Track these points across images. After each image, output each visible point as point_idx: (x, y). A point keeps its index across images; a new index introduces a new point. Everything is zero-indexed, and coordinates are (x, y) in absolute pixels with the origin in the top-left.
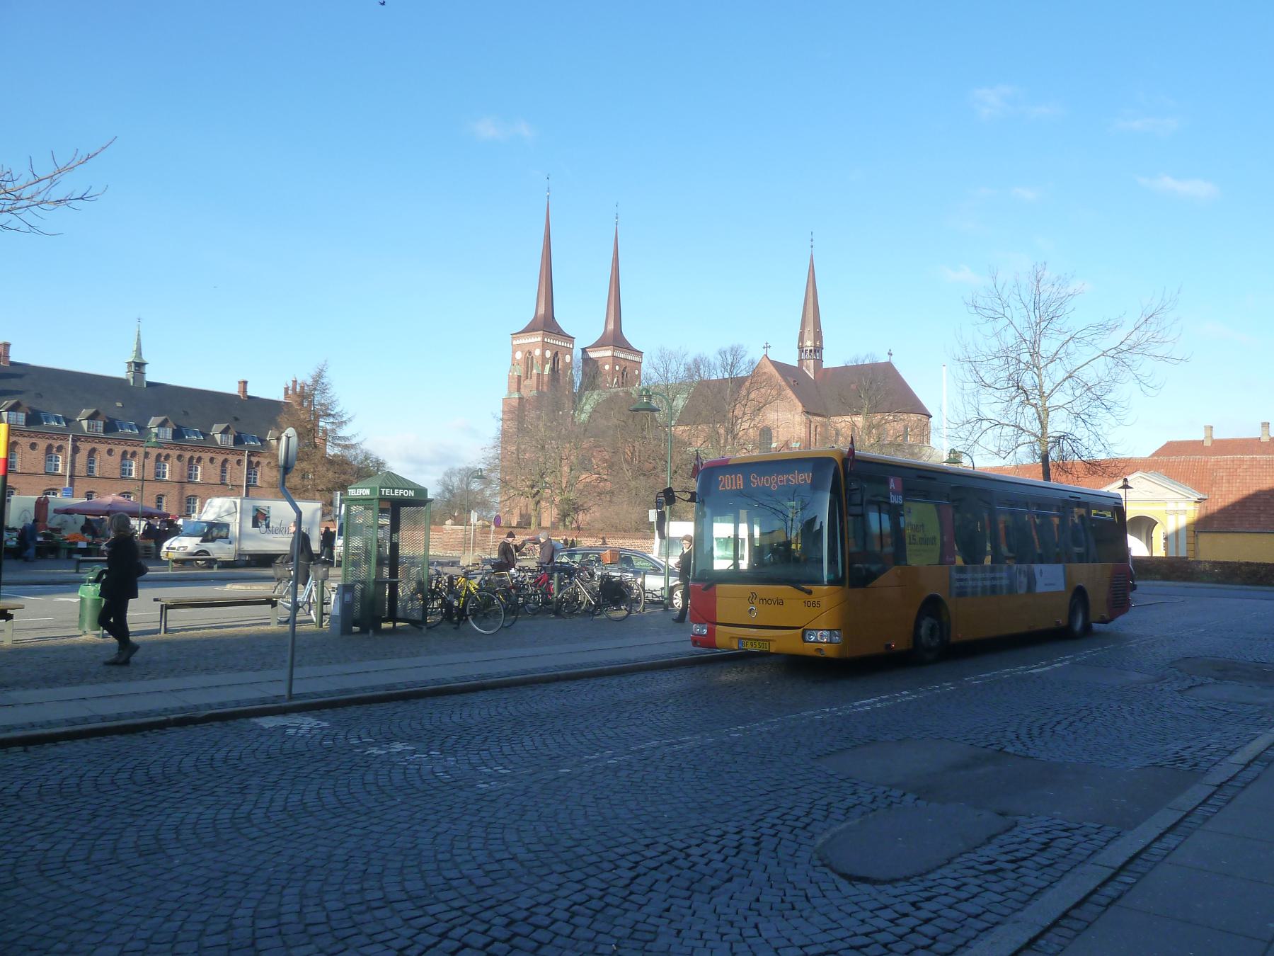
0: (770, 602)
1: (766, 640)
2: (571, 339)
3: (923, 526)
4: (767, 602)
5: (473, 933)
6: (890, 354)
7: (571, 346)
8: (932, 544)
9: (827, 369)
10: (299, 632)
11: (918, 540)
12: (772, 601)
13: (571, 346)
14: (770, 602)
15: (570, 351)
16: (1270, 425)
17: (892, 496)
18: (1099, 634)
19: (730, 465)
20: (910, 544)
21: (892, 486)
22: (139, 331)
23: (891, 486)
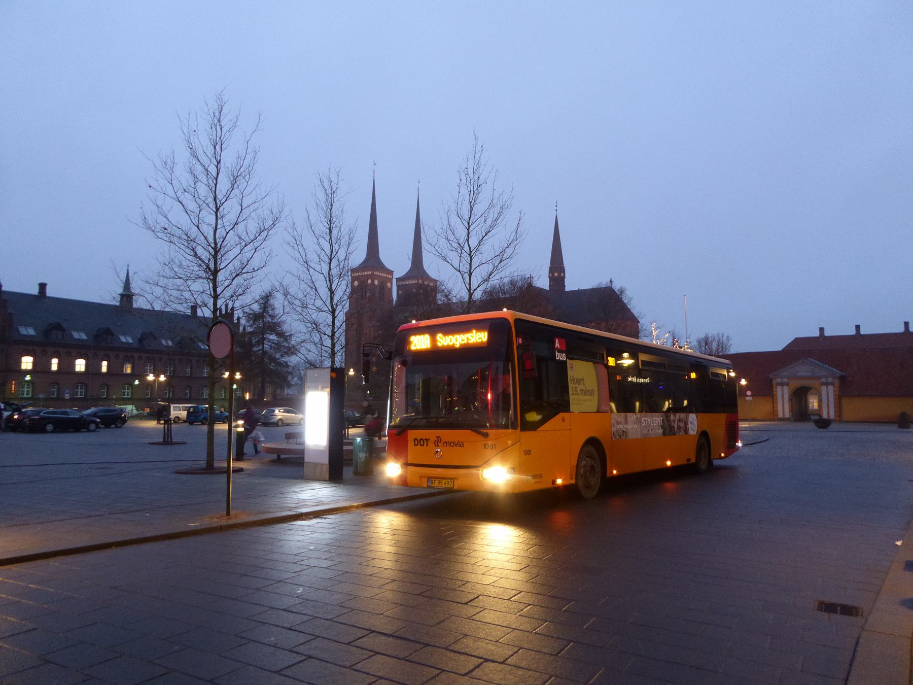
0: (452, 444)
1: (451, 479)
2: (391, 272)
3: (583, 379)
4: (450, 445)
5: (347, 642)
6: (611, 282)
7: (391, 277)
8: (591, 395)
9: (550, 285)
10: (323, 388)
11: (579, 392)
12: (454, 443)
13: (391, 277)
14: (452, 444)
15: (391, 280)
16: (673, 436)
17: (557, 354)
18: (720, 468)
19: (420, 327)
20: (573, 394)
21: (557, 345)
22: (128, 270)
23: (556, 345)
